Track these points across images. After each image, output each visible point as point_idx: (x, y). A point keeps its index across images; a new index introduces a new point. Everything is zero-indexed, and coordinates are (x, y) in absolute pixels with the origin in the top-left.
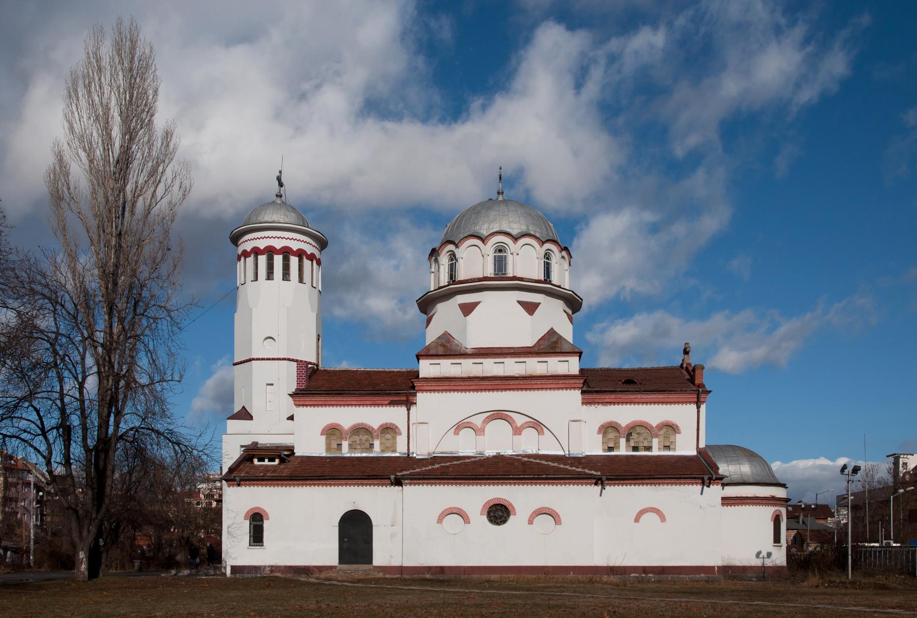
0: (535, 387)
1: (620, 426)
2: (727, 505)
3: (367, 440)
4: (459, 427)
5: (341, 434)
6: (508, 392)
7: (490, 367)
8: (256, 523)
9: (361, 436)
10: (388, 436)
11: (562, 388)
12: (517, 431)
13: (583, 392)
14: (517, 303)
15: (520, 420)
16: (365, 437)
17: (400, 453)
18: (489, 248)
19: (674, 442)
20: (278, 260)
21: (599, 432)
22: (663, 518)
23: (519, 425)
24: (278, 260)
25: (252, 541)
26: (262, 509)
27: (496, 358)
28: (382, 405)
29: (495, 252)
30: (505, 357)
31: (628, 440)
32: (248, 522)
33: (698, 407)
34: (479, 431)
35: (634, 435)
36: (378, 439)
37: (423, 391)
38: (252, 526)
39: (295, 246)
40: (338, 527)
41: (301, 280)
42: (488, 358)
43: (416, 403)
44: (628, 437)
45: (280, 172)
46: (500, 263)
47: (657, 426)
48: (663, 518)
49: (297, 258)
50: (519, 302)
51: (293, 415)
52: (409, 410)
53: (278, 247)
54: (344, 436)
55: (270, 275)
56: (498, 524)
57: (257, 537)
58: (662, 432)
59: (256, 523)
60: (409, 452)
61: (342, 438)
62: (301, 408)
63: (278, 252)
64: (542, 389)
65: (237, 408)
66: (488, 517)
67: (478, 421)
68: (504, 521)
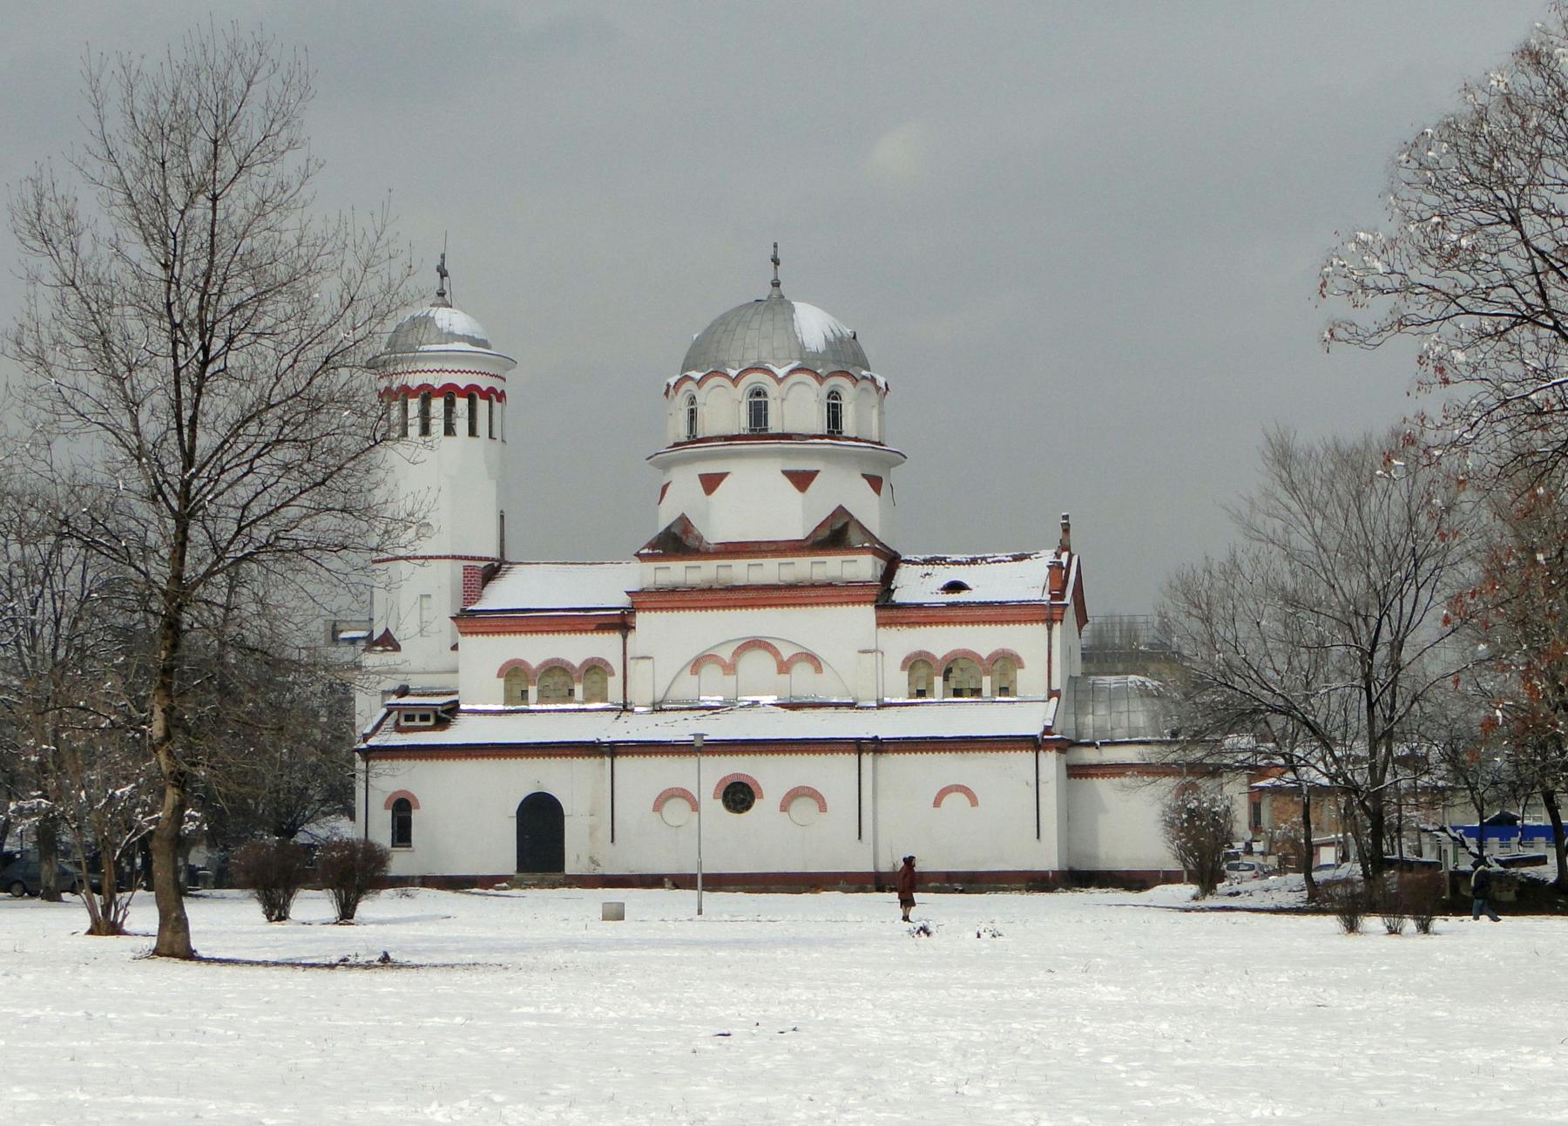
0: (807, 601)
1: (933, 657)
3: (565, 684)
4: (697, 664)
5: (526, 675)
6: (768, 609)
7: (741, 571)
9: (556, 678)
10: (596, 678)
11: (847, 603)
12: (784, 667)
13: (877, 607)
15: (786, 653)
16: (563, 679)
17: (612, 703)
18: (741, 392)
19: (1014, 682)
20: (438, 405)
21: (903, 668)
22: (974, 801)
23: (785, 659)
25: (396, 841)
26: (413, 796)
27: (750, 558)
28: (586, 631)
29: (751, 396)
30: (764, 557)
31: (946, 679)
33: (1050, 629)
34: (730, 668)
35: (956, 672)
36: (580, 682)
37: (644, 610)
38: (396, 819)
39: (462, 381)
40: (515, 819)
41: (472, 432)
42: (738, 558)
43: (634, 628)
44: (947, 674)
45: (443, 257)
46: (758, 412)
47: (990, 657)
48: (974, 801)
49: (466, 400)
50: (784, 472)
52: (625, 638)
54: (530, 678)
56: (740, 812)
58: (997, 666)
60: (625, 702)
62: (469, 636)
64: (817, 604)
65: (378, 633)
66: (724, 801)
67: (726, 654)
68: (748, 807)
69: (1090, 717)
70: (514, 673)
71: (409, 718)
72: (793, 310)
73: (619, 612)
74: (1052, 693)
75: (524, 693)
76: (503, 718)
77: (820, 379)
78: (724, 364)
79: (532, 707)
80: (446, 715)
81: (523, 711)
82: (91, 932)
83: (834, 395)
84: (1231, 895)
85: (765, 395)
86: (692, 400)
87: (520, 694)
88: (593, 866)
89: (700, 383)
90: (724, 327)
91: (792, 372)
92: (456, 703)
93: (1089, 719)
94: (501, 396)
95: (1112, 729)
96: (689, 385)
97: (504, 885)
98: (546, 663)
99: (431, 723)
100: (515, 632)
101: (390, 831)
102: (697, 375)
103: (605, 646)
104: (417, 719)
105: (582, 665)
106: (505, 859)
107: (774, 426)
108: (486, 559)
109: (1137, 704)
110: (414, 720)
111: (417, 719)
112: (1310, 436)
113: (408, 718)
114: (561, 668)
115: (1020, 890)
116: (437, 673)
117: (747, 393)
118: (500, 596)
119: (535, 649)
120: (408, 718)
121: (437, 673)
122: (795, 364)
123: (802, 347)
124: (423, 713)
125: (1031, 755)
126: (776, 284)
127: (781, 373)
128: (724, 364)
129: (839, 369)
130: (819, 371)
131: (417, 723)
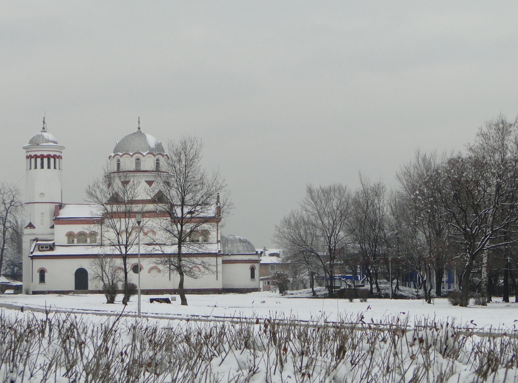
2: (225, 263)
5: (74, 236)
8: (42, 274)
10: (93, 236)
14: (145, 182)
20: (46, 160)
24: (46, 160)
26: (40, 268)
29: (136, 160)
32: (39, 273)
39: (52, 154)
41: (55, 168)
49: (53, 159)
51: (187, 305)
53: (45, 155)
55: (42, 167)
57: (42, 279)
59: (42, 274)
61: (74, 238)
63: (45, 157)
69: (227, 247)
70: (70, 235)
71: (42, 247)
72: (145, 136)
73: (100, 219)
74: (218, 242)
75: (73, 241)
76: (68, 248)
77: (154, 156)
78: (128, 151)
79: (75, 244)
80: (52, 247)
81: (72, 246)
82: (107, 303)
83: (158, 160)
84: (291, 294)
85: (140, 160)
86: (119, 160)
87: (72, 241)
88: (96, 288)
89: (121, 156)
90: (127, 141)
91: (147, 154)
92: (54, 243)
93: (227, 248)
94: (60, 157)
95: (233, 251)
96: (117, 157)
97: (72, 293)
98: (79, 232)
99: (48, 249)
100: (70, 224)
101: (39, 278)
102: (121, 154)
103: (95, 228)
104: (45, 248)
105: (89, 234)
106: (71, 286)
107: (142, 168)
108: (59, 203)
109: (239, 244)
110: (43, 248)
111: (45, 248)
112: (316, 186)
113: (41, 248)
114: (84, 234)
115: (213, 293)
116: (46, 234)
117: (135, 159)
118: (64, 213)
119: (76, 229)
120: (41, 248)
121: (46, 234)
122: (148, 152)
123: (149, 147)
124: (46, 246)
125: (215, 258)
126: (139, 128)
127: (144, 154)
128: (128, 151)
129: (159, 153)
130: (154, 154)
131: (45, 249)
